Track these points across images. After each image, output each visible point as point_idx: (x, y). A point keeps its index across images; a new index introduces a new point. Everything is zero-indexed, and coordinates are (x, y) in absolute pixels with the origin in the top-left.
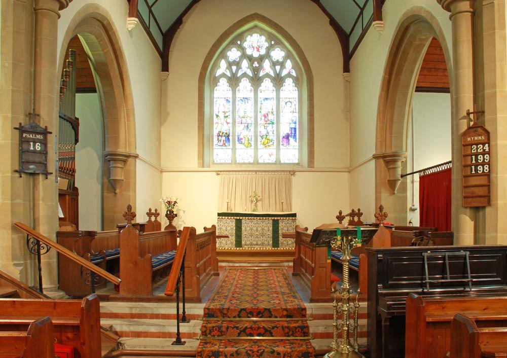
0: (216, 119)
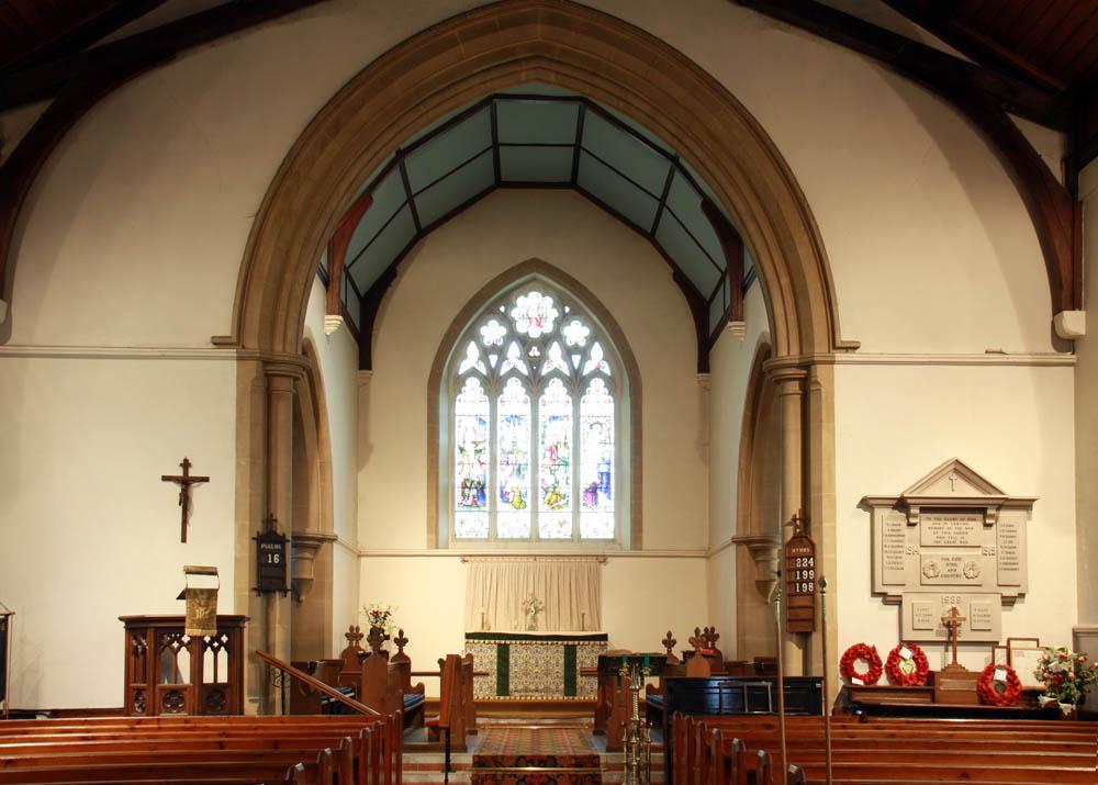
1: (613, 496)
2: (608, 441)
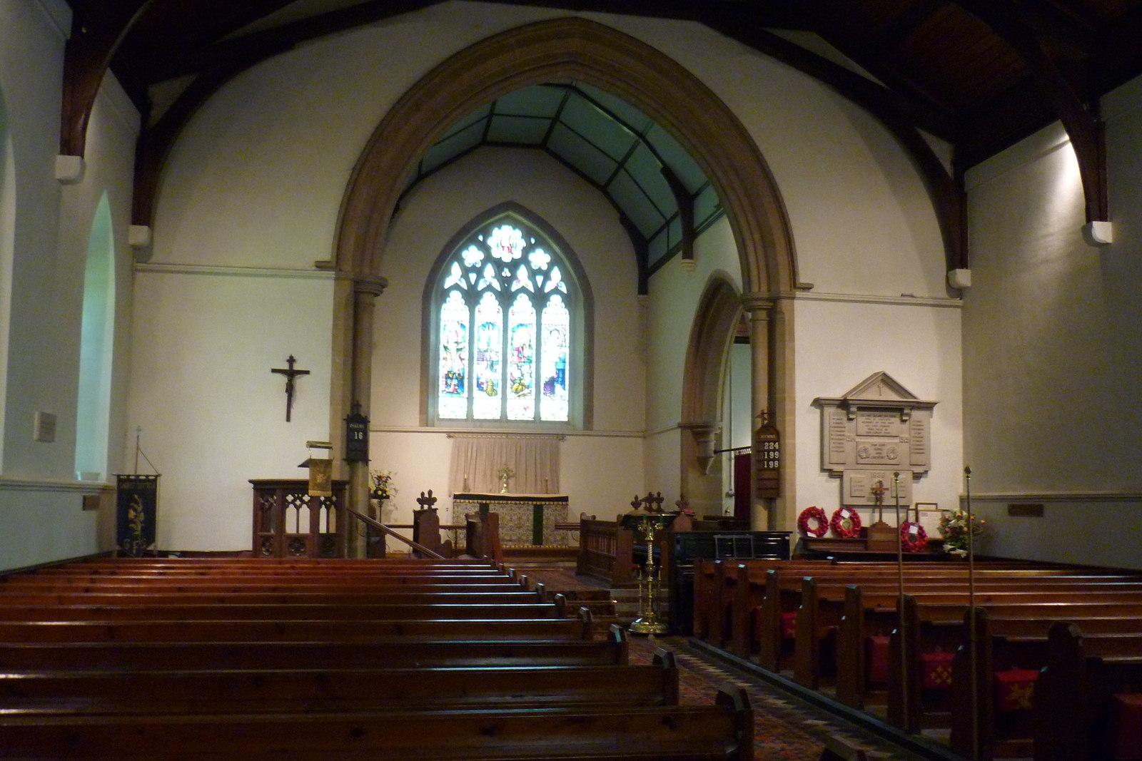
0: (445, 352)
1: (567, 387)
2: (564, 344)
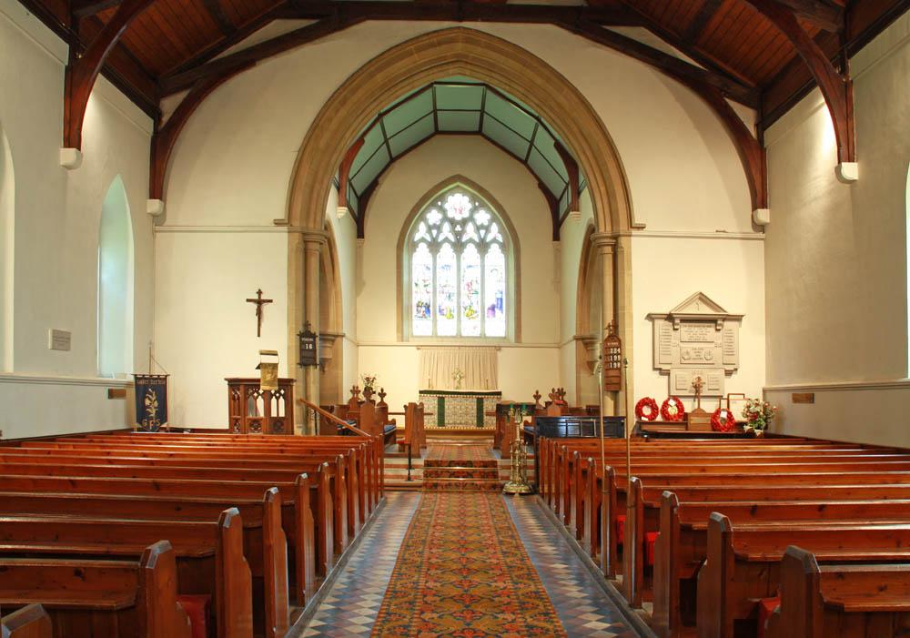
1: (504, 312)
